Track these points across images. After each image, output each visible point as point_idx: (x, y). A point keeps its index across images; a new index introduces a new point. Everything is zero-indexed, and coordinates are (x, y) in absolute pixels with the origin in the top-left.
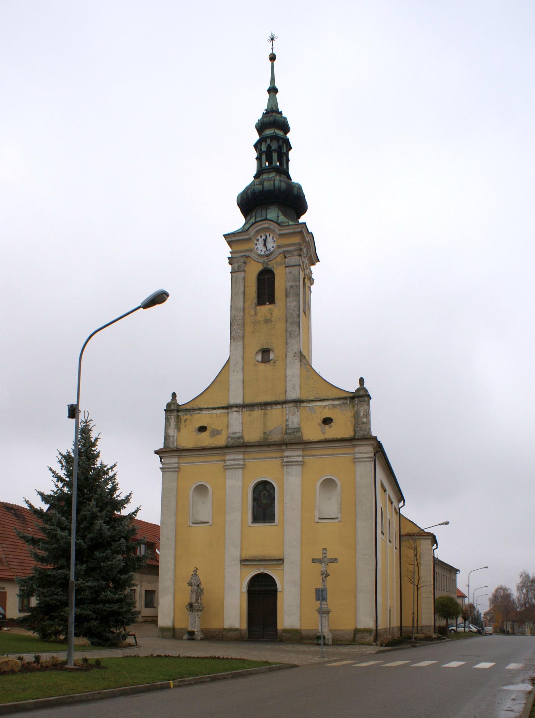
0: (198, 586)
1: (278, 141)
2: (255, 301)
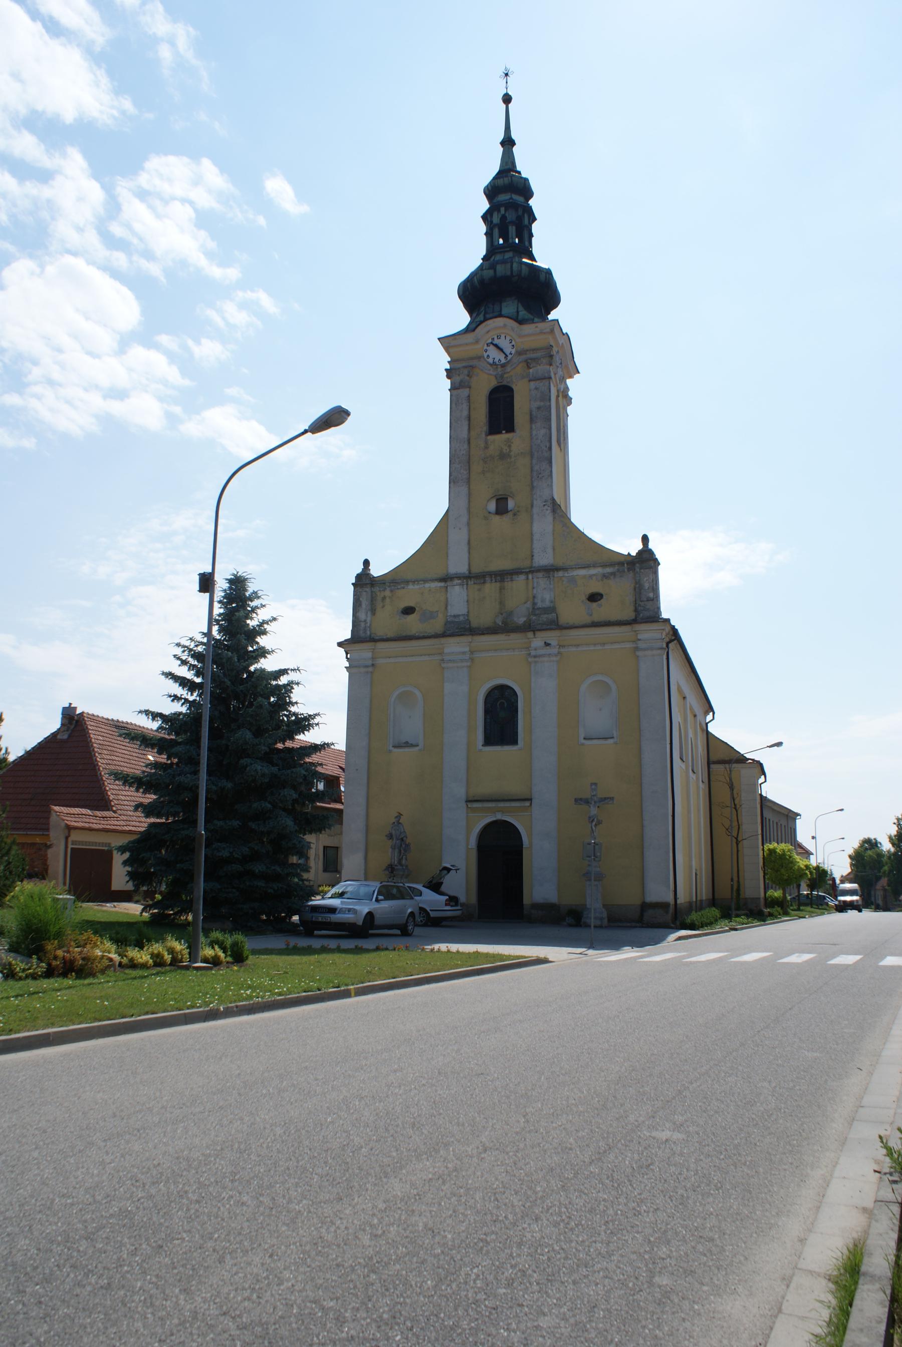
1: (517, 210)
2: (485, 428)
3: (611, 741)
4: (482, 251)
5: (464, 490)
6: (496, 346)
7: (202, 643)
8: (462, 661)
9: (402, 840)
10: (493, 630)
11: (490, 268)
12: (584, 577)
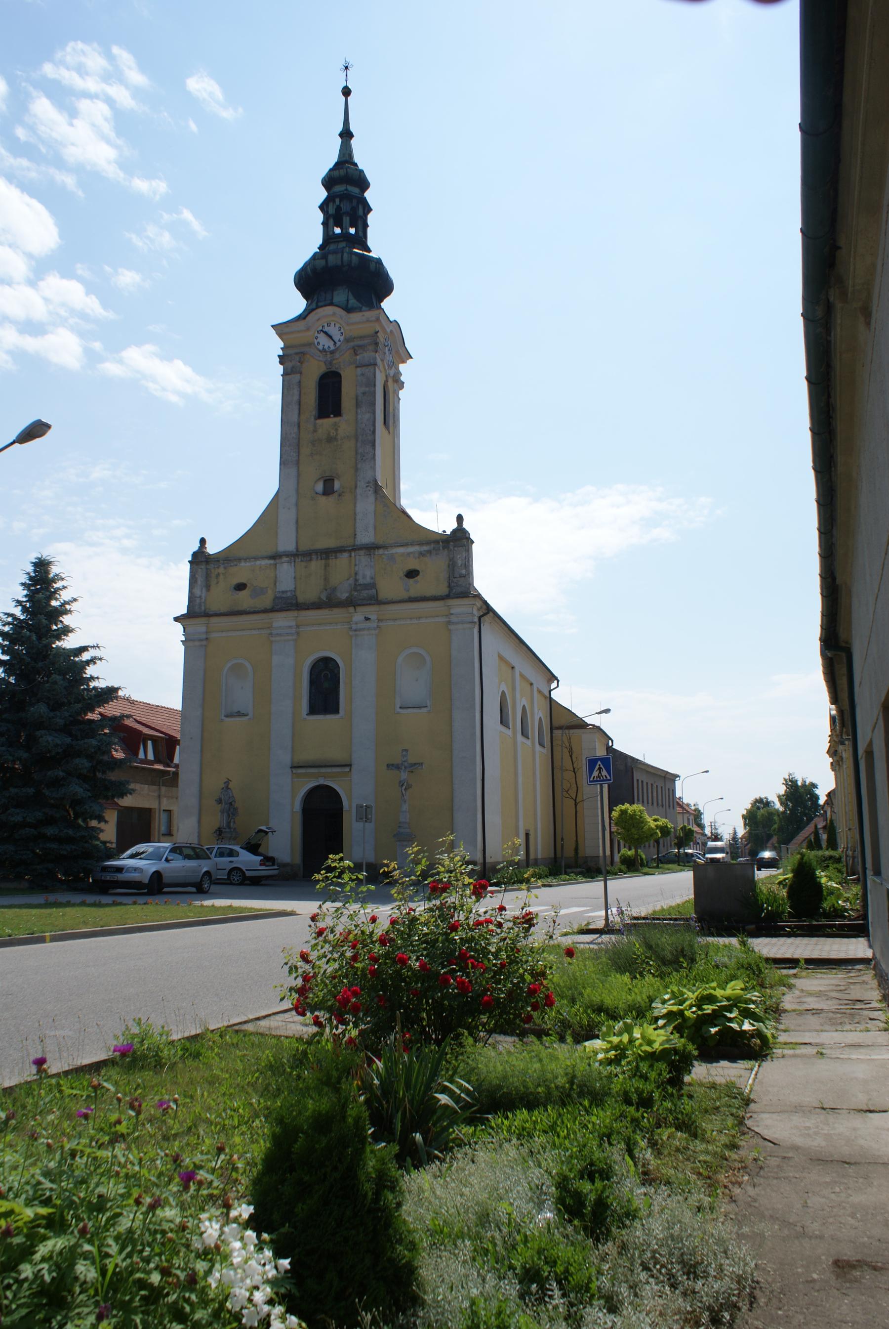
0: (231, 804)
1: (351, 202)
2: (314, 412)
3: (424, 710)
4: (319, 241)
5: (293, 471)
6: (326, 333)
7: (9, 623)
8: (288, 634)
9: (231, 804)
10: (317, 605)
11: (322, 258)
12: (402, 555)
